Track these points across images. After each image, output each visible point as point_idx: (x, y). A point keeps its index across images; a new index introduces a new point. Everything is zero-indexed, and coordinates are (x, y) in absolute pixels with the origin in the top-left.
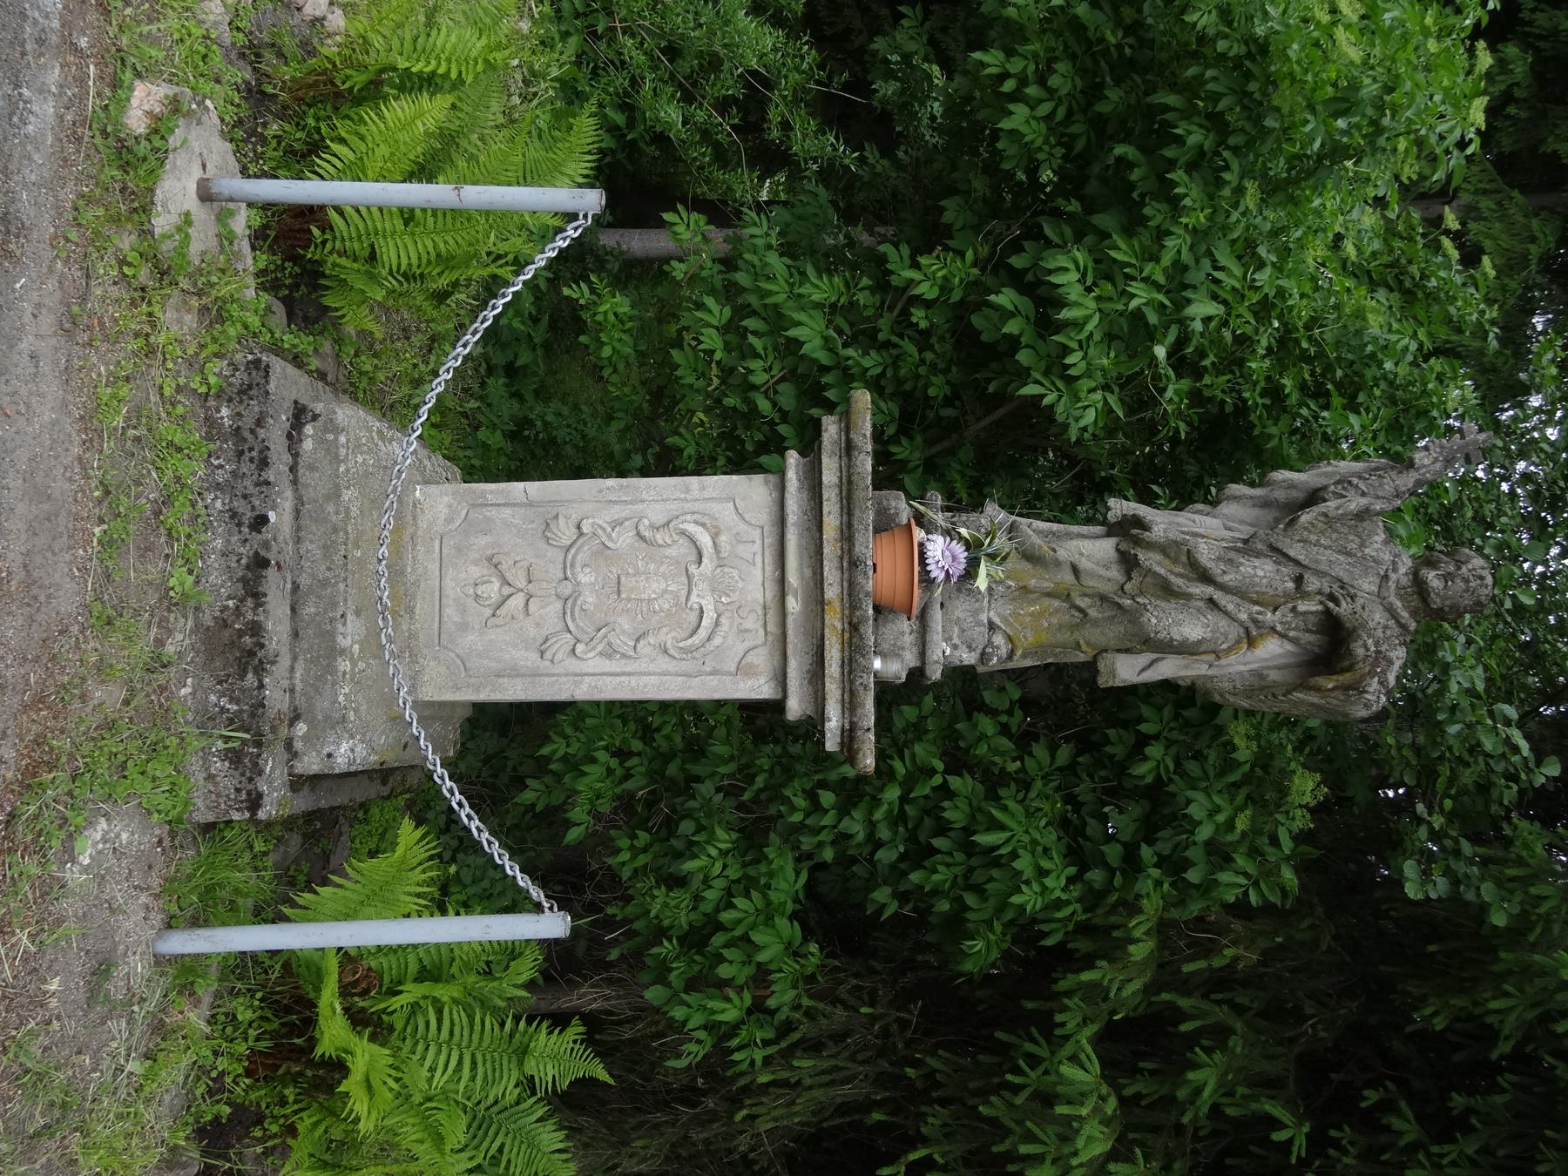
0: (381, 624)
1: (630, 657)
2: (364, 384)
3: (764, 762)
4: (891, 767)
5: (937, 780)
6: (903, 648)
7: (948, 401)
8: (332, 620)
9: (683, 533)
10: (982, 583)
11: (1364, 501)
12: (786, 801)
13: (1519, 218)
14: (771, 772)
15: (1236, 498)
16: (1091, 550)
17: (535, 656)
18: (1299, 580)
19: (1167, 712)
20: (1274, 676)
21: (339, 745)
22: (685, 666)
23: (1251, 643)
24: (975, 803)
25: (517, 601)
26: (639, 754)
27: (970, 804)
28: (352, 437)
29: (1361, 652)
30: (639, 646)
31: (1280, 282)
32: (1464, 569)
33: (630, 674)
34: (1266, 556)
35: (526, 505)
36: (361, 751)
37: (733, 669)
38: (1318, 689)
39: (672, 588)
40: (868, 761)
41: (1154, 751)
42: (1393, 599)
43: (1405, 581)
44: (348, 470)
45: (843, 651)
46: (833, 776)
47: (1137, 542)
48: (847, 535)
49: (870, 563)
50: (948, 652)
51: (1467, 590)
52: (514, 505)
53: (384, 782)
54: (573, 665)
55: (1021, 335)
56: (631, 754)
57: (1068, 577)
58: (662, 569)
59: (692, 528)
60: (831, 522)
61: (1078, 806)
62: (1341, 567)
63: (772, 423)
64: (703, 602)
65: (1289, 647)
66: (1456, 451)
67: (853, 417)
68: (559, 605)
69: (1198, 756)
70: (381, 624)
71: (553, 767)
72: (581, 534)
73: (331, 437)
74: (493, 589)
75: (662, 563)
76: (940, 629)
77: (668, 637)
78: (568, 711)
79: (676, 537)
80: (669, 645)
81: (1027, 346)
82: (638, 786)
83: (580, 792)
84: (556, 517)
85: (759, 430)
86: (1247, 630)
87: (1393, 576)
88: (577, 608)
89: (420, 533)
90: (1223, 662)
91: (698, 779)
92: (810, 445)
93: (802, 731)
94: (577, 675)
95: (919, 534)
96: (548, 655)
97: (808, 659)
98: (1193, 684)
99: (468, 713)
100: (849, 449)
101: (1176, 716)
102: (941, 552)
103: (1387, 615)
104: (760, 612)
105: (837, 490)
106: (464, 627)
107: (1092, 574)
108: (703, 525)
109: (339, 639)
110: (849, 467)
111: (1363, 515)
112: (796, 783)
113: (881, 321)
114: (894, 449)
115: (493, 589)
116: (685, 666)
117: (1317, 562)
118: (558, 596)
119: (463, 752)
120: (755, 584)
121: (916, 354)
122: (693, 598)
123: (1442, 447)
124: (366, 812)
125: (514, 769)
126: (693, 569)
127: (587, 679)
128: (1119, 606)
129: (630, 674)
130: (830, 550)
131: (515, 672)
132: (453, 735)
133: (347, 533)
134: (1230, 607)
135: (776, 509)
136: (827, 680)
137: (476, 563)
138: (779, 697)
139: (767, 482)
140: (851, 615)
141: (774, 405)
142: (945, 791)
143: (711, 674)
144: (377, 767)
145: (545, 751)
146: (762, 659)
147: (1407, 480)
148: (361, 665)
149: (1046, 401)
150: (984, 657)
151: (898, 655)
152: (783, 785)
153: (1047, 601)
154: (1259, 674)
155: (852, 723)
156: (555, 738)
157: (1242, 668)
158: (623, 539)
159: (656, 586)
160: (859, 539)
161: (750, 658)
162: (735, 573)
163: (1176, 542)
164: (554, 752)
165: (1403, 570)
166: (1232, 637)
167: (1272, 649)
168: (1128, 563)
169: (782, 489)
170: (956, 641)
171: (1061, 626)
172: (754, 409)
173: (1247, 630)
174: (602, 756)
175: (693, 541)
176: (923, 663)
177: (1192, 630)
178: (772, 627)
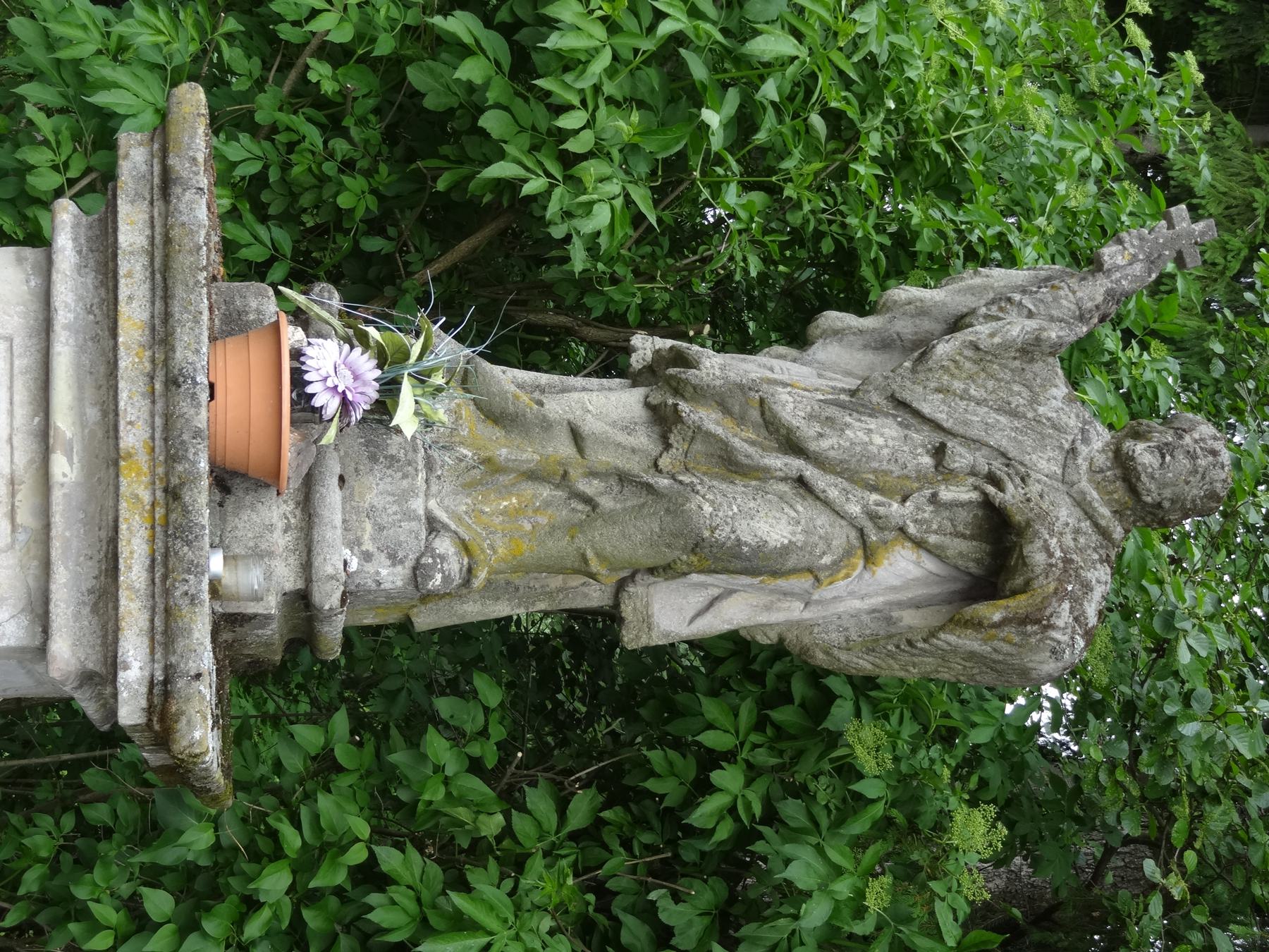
5: (357, 855)
7: (375, 226)
10: (405, 417)
11: (1032, 324)
12: (82, 913)
13: (1237, 152)
15: (837, 334)
16: (606, 408)
18: (939, 452)
19: (747, 711)
20: (909, 618)
23: (869, 555)
24: (426, 896)
27: (419, 900)
29: (1039, 558)
31: (895, 38)
32: (1187, 439)
34: (887, 415)
38: (977, 625)
41: (728, 778)
42: (1085, 485)
43: (1102, 460)
45: (152, 540)
47: (678, 388)
48: (162, 335)
49: (202, 379)
50: (354, 565)
51: (1195, 472)
55: (486, 85)
57: (564, 448)
60: (134, 312)
61: (604, 895)
62: (1003, 433)
65: (930, 564)
66: (1164, 246)
69: (800, 791)
76: (338, 518)
81: (497, 106)
86: (862, 533)
87: (1083, 450)
90: (826, 592)
95: (292, 335)
97: (91, 569)
98: (781, 640)
100: (165, 185)
101: (760, 724)
102: (336, 367)
103: (1078, 513)
105: (144, 260)
107: (605, 442)
110: (166, 215)
111: (1029, 350)
113: (261, 98)
117: (966, 423)
121: (319, 142)
123: (1141, 239)
128: (649, 488)
134: (833, 494)
135: (35, 306)
136: (123, 595)
139: (20, 260)
142: (371, 876)
147: (1093, 291)
149: (527, 189)
150: (418, 573)
153: (529, 489)
154: (883, 615)
155: (169, 669)
157: (857, 604)
160: (183, 337)
163: (741, 387)
165: (1097, 444)
166: (839, 543)
167: (902, 569)
168: (663, 420)
169: (47, 271)
170: (368, 546)
171: (553, 528)
173: (862, 533)
176: (308, 580)
177: (770, 524)
178: (25, 517)
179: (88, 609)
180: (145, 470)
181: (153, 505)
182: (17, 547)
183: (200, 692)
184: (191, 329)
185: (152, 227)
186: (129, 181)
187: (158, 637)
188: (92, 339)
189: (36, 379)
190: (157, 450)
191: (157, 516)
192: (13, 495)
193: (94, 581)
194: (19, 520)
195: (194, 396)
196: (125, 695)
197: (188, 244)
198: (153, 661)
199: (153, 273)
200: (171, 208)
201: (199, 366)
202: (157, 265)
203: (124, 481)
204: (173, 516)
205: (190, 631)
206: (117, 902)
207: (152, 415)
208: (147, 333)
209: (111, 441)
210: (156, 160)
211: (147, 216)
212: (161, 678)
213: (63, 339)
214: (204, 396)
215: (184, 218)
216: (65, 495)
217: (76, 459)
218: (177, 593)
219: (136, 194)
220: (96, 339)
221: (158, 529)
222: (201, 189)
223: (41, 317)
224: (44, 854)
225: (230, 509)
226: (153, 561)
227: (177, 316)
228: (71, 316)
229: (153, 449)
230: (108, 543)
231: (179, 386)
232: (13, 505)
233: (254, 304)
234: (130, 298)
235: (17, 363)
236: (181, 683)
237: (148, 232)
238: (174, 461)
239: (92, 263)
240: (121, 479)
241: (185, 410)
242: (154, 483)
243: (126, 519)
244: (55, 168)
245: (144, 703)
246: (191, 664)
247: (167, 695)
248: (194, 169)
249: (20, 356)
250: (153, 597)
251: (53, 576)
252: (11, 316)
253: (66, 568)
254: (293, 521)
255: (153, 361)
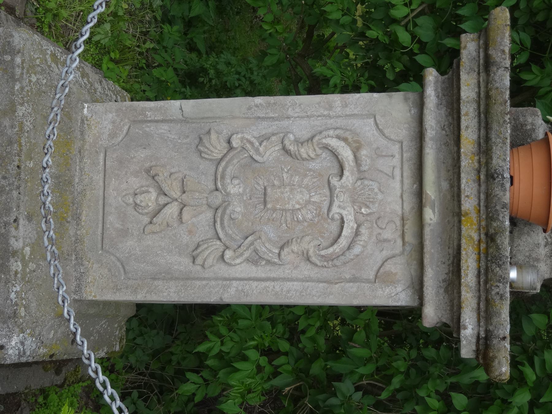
0: (43, 226)
1: (275, 264)
2: (49, 18)
3: (401, 365)
4: (521, 373)
6: (538, 260)
8: (6, 224)
9: (326, 147)
14: (407, 374)
17: (186, 261)
21: (10, 338)
22: (326, 273)
25: (172, 210)
26: (286, 354)
28: (27, 59)
30: (283, 253)
33: (274, 280)
35: (181, 121)
36: (30, 344)
37: (372, 277)
39: (315, 199)
40: (503, 369)
44: (22, 88)
45: (479, 260)
46: (465, 379)
48: (485, 149)
49: (507, 175)
52: (171, 121)
53: (58, 372)
54: (222, 270)
56: (279, 353)
58: (306, 181)
59: (334, 143)
63: (411, 54)
64: (344, 213)
67: (492, 34)
68: (209, 214)
70: (43, 226)
71: (209, 362)
72: (231, 148)
73: (8, 58)
74: (151, 199)
75: (305, 176)
77: (309, 245)
78: (223, 313)
79: (319, 151)
80: (311, 253)
82: (285, 382)
83: (232, 387)
84: (209, 132)
85: (399, 60)
88: (226, 217)
89: (87, 147)
91: (339, 378)
92: (448, 61)
93: (435, 337)
94: (226, 279)
96: (199, 261)
99: (132, 312)
100: (487, 65)
104: (398, 223)
105: (475, 106)
106: (124, 233)
108: (345, 140)
109: (12, 241)
110: (487, 83)
112: (430, 385)
114: (525, 76)
115: (151, 199)
116: (326, 273)
118: (209, 206)
119: (131, 347)
120: (393, 195)
122: (335, 209)
124: (45, 398)
125: (179, 363)
126: (334, 181)
127: (235, 283)
129: (274, 280)
130: (468, 162)
131: (168, 275)
132: (118, 331)
133: (20, 145)
136: (463, 289)
137: (136, 174)
138: (415, 304)
139: (406, 99)
140: (487, 226)
141: (414, 37)
143: (350, 281)
144: (47, 359)
145: (201, 348)
146: (400, 268)
148: (32, 266)
151: (534, 267)
152: (418, 386)
155: (487, 331)
156: (211, 336)
158: (270, 153)
159: (299, 197)
161: (389, 267)
162: (375, 186)
164: (210, 350)
169: (421, 105)
172: (395, 40)
174: (253, 354)
175: (335, 155)
178: (410, 238)
179: (443, 290)
180: (475, 222)
181: (480, 241)
182: (406, 254)
183: (505, 347)
184: (501, 147)
185: (479, 87)
186: (467, 61)
187: (482, 314)
188: (445, 144)
189: (415, 164)
190: (482, 212)
191: (482, 248)
192: (403, 225)
193: (446, 276)
194: (407, 239)
195: (502, 185)
196: (464, 342)
197: (500, 100)
198: (479, 325)
199: (479, 113)
200: (491, 79)
201: (505, 168)
202: (482, 110)
203: (464, 228)
204: (491, 250)
205: (500, 314)
206: (438, 397)
207: (479, 193)
208: (476, 146)
209: (456, 203)
210: (481, 50)
211: (476, 81)
212: (484, 336)
213: (430, 146)
214: (508, 185)
215: (498, 85)
216: (431, 230)
217: (436, 211)
218: (493, 293)
219: (470, 68)
220: (446, 144)
221: (482, 255)
222: (506, 68)
223: (417, 130)
224: (402, 370)
225: (516, 235)
226: (479, 272)
227: (493, 140)
228: (434, 132)
229: (479, 211)
230: (454, 257)
231: (495, 179)
232: (403, 231)
233: (530, 120)
234: (467, 127)
235: (405, 155)
236: (495, 341)
237: (477, 90)
238: (492, 220)
239: (444, 102)
240: (462, 227)
241: (498, 193)
242: (479, 230)
243: (465, 249)
244: (406, 5)
245: (474, 348)
246: (500, 331)
247: (487, 346)
248: (503, 56)
249: (406, 151)
250: (479, 291)
251: (426, 273)
252: (402, 130)
253: (432, 269)
254: (549, 240)
255: (479, 162)
